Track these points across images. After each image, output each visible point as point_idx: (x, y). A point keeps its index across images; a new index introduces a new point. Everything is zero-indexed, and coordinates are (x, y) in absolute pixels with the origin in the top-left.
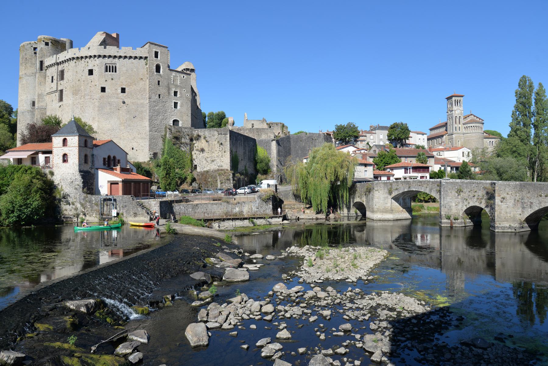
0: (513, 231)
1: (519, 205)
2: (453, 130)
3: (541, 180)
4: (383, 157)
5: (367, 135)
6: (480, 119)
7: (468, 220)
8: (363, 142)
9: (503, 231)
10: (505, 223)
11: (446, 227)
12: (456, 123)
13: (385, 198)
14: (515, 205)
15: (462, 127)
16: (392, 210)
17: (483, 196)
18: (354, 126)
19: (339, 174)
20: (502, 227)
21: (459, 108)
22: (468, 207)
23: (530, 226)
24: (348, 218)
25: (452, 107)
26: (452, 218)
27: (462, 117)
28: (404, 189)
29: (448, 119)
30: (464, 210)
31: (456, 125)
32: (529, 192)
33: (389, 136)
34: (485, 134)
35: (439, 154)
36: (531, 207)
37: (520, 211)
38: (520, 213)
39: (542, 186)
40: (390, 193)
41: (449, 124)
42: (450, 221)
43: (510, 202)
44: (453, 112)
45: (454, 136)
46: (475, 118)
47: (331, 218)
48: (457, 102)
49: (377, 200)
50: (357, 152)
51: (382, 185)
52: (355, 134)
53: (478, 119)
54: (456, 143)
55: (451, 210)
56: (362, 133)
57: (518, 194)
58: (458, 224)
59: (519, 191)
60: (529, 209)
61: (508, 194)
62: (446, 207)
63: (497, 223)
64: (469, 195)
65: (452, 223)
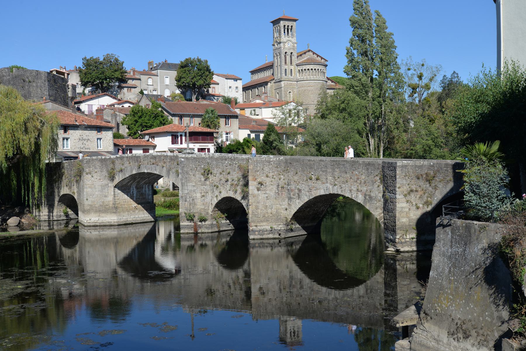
0: (277, 236)
1: (285, 194)
2: (281, 74)
3: (390, 155)
4: (139, 114)
5: (143, 77)
6: (322, 58)
7: (224, 221)
8: (133, 90)
9: (261, 237)
10: (264, 224)
11: (188, 233)
12: (286, 63)
13: (104, 187)
14: (279, 194)
15: (295, 69)
16: (116, 208)
17: (239, 180)
18: (117, 60)
19: (21, 143)
20: (260, 231)
21: (290, 39)
22: (220, 198)
23: (304, 228)
24: (49, 223)
25: (280, 37)
26: (196, 219)
27: (295, 55)
28: (132, 171)
29: (274, 57)
30: (214, 204)
31: (286, 67)
32: (297, 173)
33: (178, 79)
34: (329, 82)
35: (253, 112)
36: (299, 197)
37: (285, 204)
38: (286, 206)
39: (312, 163)
40: (112, 178)
41: (276, 65)
42: (193, 224)
43: (271, 190)
44: (282, 44)
45: (282, 83)
46: (315, 56)
47: (10, 225)
48: (288, 30)
49: (89, 190)
50: (116, 106)
51: (98, 164)
52: (117, 75)
53: (319, 59)
54: (286, 96)
55: (195, 204)
56: (134, 74)
57: (282, 176)
58: (207, 228)
59: (284, 171)
60: (297, 201)
61: (267, 176)
62: (186, 201)
63: (253, 224)
64: (221, 180)
65: (196, 227)
